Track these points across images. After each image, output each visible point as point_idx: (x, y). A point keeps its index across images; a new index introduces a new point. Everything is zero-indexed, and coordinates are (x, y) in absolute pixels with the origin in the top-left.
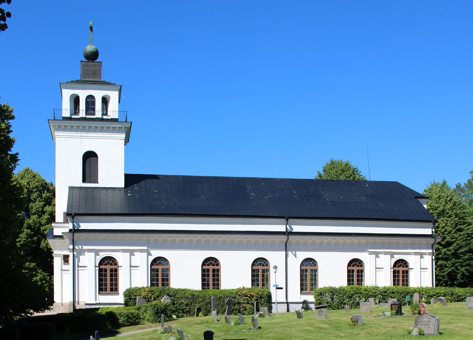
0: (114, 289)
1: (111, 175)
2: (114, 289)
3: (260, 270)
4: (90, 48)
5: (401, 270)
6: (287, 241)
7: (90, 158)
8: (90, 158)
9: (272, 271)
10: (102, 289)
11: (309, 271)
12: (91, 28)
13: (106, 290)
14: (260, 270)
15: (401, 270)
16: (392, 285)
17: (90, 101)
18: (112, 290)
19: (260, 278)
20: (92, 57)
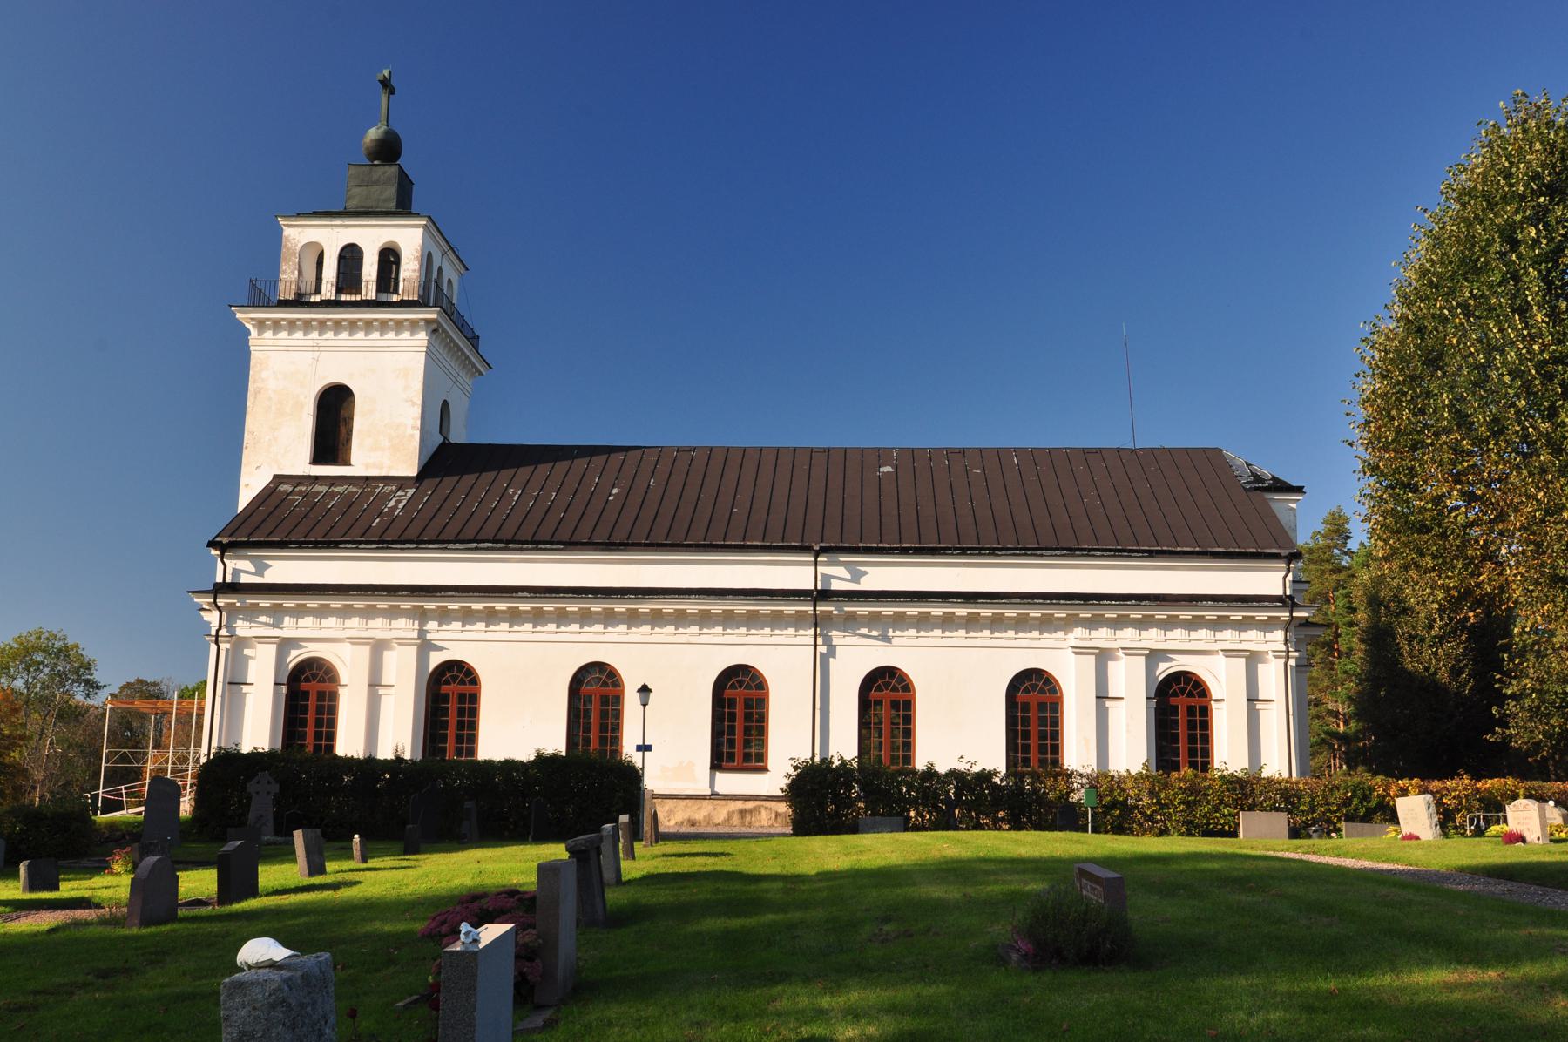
0: (755, 761)
1: (387, 445)
2: (755, 761)
3: (595, 696)
4: (373, 134)
5: (1179, 709)
6: (821, 608)
7: (334, 408)
8: (334, 408)
9: (631, 700)
10: (721, 759)
11: (886, 704)
12: (385, 83)
13: (731, 757)
14: (595, 696)
15: (1179, 709)
16: (1302, 773)
17: (389, 257)
18: (747, 757)
19: (739, 724)
20: (388, 150)
